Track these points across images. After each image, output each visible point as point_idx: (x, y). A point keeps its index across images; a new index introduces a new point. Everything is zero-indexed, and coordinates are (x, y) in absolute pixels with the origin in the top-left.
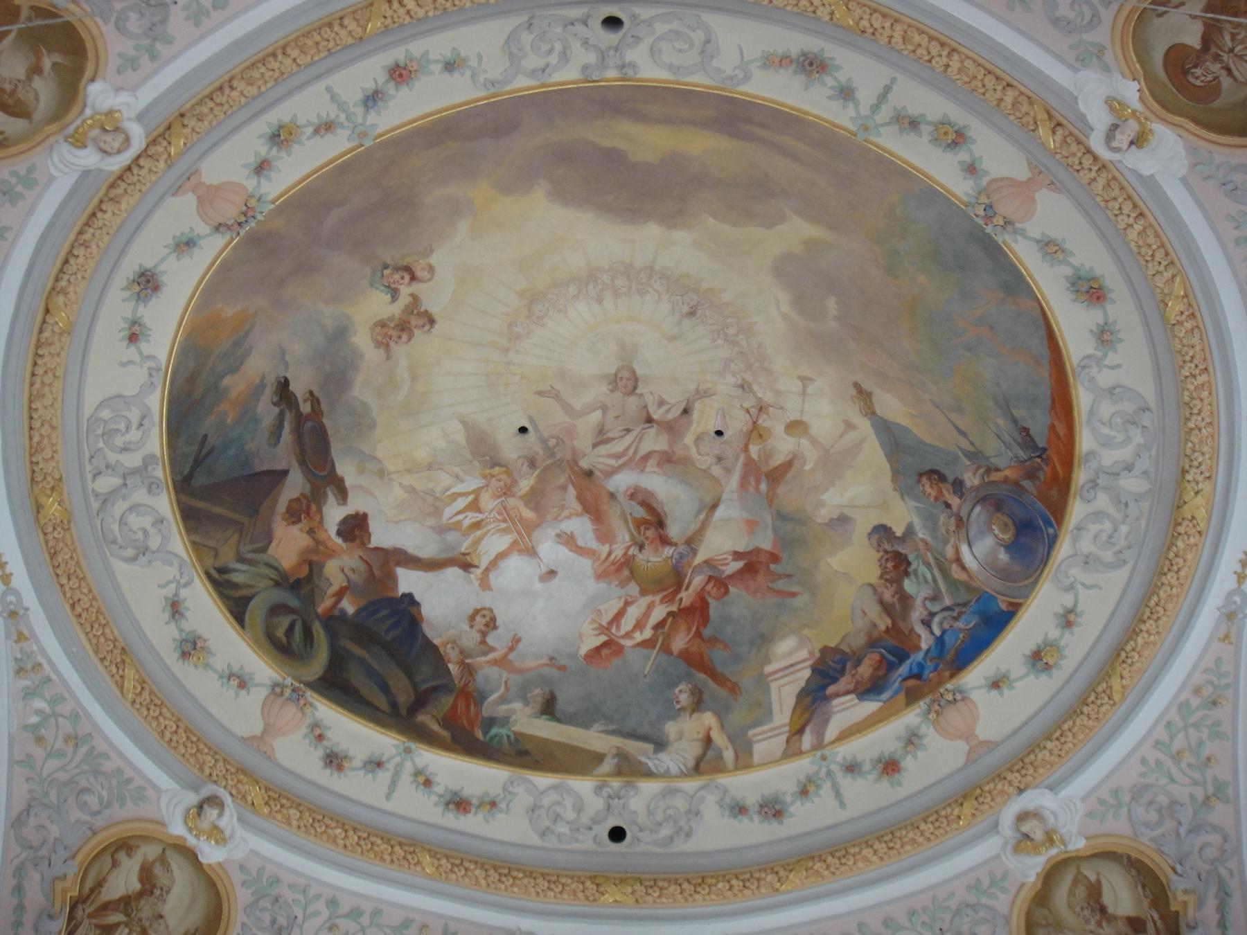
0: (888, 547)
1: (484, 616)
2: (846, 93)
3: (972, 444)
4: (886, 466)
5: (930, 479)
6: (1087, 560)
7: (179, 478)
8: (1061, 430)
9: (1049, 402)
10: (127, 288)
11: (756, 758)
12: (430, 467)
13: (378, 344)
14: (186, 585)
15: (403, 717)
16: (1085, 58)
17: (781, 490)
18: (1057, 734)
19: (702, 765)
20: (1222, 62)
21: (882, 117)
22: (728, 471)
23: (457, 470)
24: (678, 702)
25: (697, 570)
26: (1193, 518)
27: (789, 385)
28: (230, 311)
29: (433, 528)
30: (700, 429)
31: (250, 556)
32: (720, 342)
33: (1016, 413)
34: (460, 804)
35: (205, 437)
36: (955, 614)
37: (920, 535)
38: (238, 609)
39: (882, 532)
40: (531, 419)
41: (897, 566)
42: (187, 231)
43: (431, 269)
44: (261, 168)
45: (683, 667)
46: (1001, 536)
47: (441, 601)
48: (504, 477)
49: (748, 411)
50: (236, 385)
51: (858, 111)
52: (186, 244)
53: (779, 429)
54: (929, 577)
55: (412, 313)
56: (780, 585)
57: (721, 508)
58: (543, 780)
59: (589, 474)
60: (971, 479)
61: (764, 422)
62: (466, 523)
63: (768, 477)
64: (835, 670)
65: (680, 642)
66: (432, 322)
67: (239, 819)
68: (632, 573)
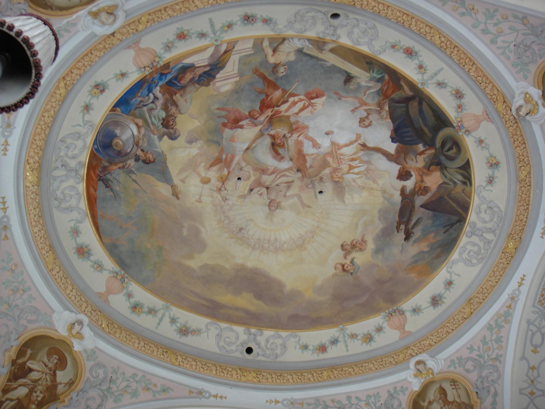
0: (171, 131)
1: (364, 124)
2: (173, 321)
3: (130, 177)
4: (169, 165)
5: (150, 160)
6: (79, 136)
7: (462, 223)
8: (92, 190)
9: (97, 201)
10: (443, 302)
11: (252, 41)
12: (364, 188)
13: (365, 242)
14: (482, 186)
15: (418, 96)
16: (93, 353)
17: (216, 155)
18: (128, 333)
19: (281, 41)
20: (49, 368)
21: (162, 312)
22: (238, 164)
23: (353, 184)
24: (285, 68)
25: (261, 123)
26: (32, 171)
27: (206, 199)
28: (413, 275)
29: (372, 164)
30: (247, 182)
31: (451, 183)
32: (232, 218)
33: (111, 193)
34: (409, 53)
35: (445, 233)
36: (142, 104)
37: (156, 137)
38: (466, 167)
39: (173, 137)
40: (316, 197)
41: (167, 123)
42: (413, 316)
43: (335, 268)
44: (379, 329)
45: (278, 83)
46: (119, 141)
47: (381, 135)
48: (335, 176)
49: (225, 189)
50: (424, 246)
51: (170, 313)
52: (416, 310)
53: (213, 181)
54: (153, 119)
55: (349, 251)
56: (224, 113)
57: (245, 148)
58: (364, 49)
59: (298, 170)
60: (131, 162)
61: (219, 184)
62: (357, 162)
63: (221, 161)
64: (204, 77)
65: (277, 94)
66: (342, 246)
67: (514, 98)
68: (291, 126)
